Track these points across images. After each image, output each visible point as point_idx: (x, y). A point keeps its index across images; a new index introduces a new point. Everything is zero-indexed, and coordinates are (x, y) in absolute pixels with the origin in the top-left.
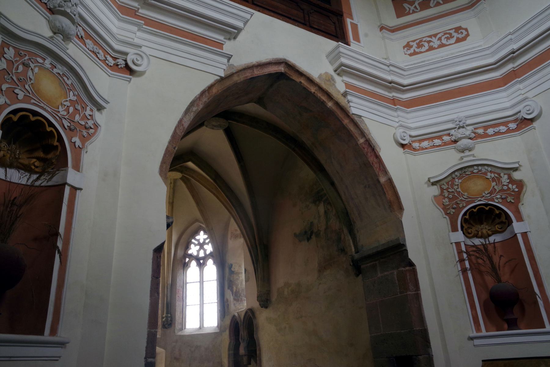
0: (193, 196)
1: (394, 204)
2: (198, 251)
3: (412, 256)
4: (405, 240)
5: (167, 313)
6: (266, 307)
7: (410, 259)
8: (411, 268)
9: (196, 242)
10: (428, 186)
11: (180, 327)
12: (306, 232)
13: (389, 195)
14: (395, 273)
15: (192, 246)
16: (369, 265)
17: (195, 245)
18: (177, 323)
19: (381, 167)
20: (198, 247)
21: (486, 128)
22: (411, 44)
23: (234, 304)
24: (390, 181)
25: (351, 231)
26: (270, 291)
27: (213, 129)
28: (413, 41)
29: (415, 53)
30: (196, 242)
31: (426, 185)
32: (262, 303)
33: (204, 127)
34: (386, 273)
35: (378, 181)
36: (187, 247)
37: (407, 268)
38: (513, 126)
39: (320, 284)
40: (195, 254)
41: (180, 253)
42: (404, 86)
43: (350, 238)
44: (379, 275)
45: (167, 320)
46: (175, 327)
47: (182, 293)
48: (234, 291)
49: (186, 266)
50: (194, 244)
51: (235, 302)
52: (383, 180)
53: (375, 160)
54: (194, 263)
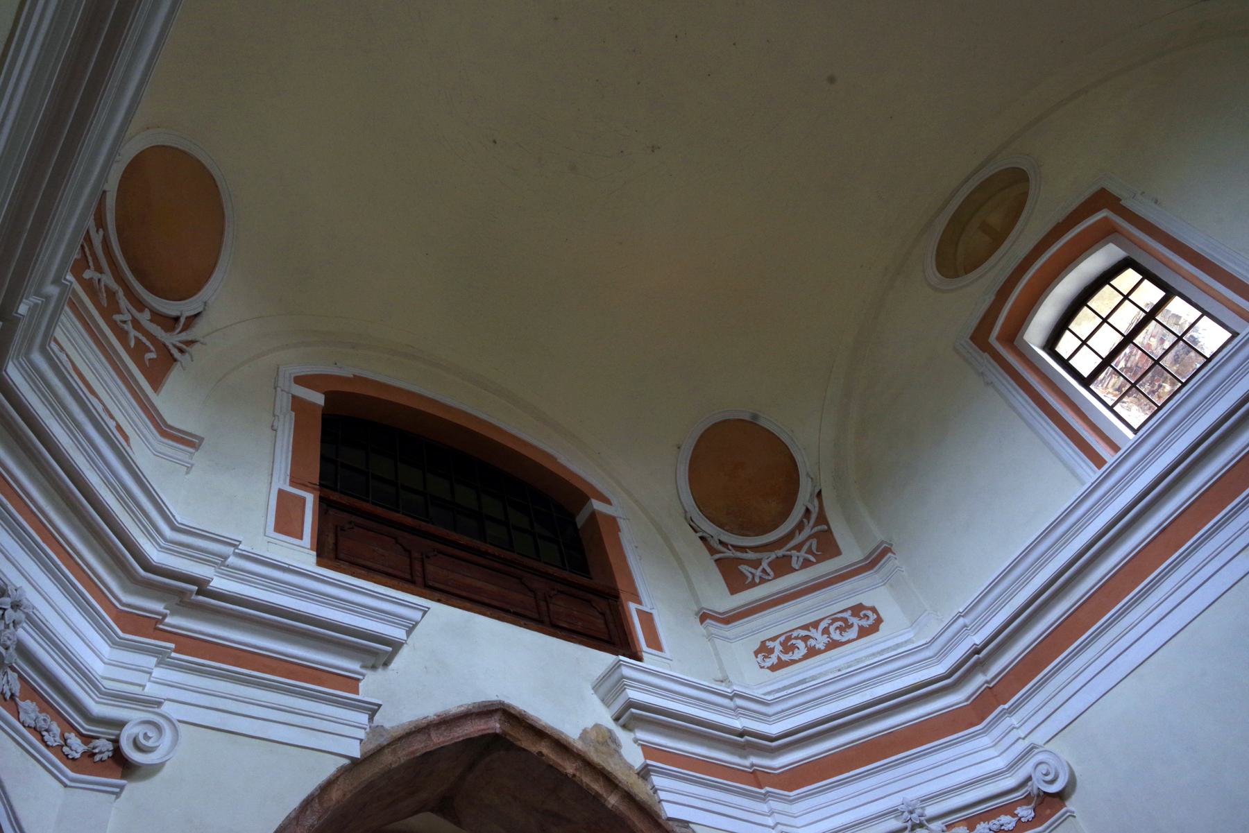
21: (31, 692)
22: (770, 644)
28: (773, 639)
29: (780, 665)
38: (77, 746)
42: (772, 739)
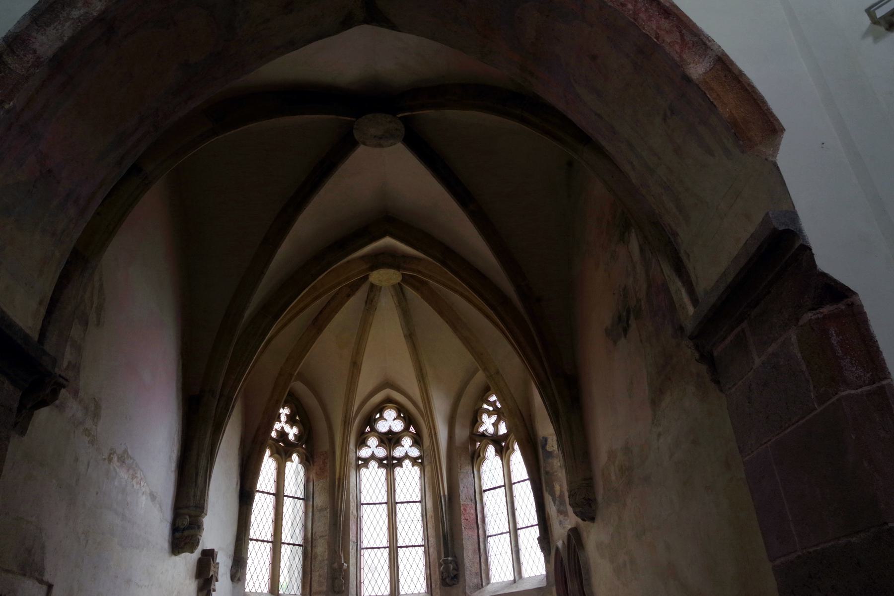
0: (441, 313)
1: (755, 123)
2: (496, 425)
3: (828, 261)
4: (793, 216)
5: (446, 555)
6: (592, 519)
7: (824, 275)
8: (842, 306)
9: (491, 409)
10: (877, 38)
11: (476, 581)
12: (620, 318)
13: (729, 106)
14: (794, 338)
15: (485, 417)
16: (727, 341)
17: (490, 414)
18: (467, 573)
19: (688, 38)
20: (494, 418)
23: (561, 523)
24: (723, 63)
25: (680, 268)
26: (591, 479)
27: (381, 146)
30: (491, 409)
31: (870, 40)
32: (578, 510)
33: (361, 151)
34: (770, 350)
35: (687, 79)
36: (476, 421)
37: (826, 310)
39: (659, 435)
40: (491, 430)
41: (462, 433)
43: (679, 284)
44: (757, 361)
45: (447, 569)
46: (465, 580)
47: (473, 512)
48: (558, 493)
49: (476, 458)
50: (487, 411)
51: (561, 517)
52: (697, 70)
53: (665, 24)
54: (491, 450)
